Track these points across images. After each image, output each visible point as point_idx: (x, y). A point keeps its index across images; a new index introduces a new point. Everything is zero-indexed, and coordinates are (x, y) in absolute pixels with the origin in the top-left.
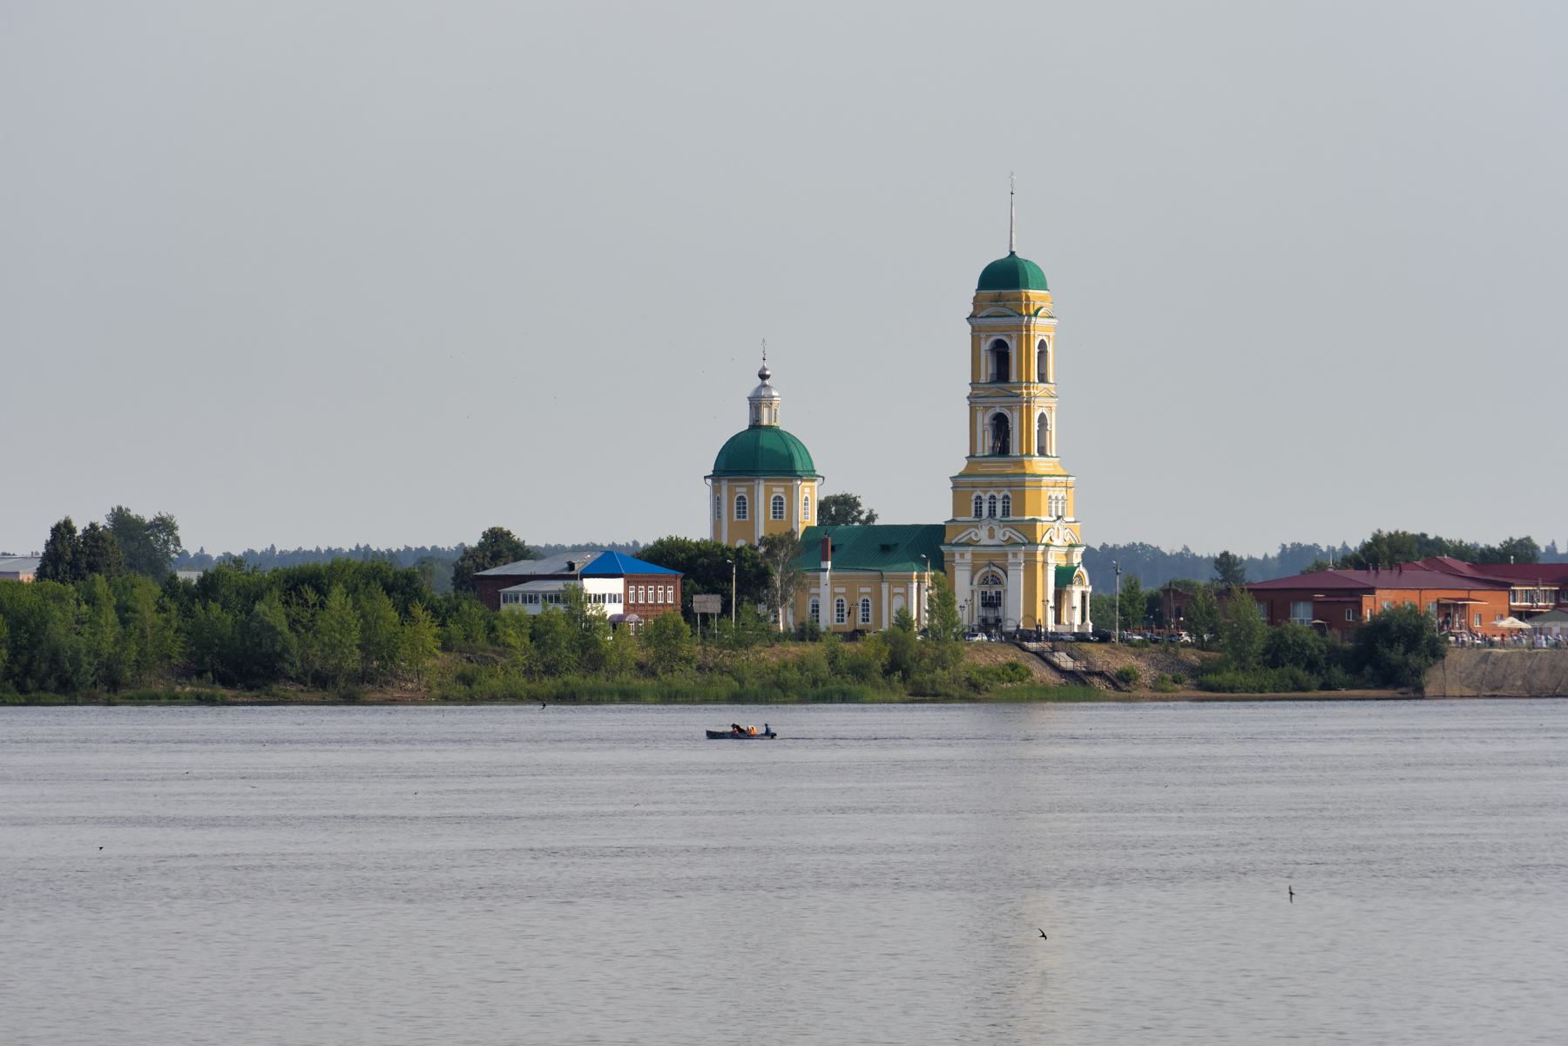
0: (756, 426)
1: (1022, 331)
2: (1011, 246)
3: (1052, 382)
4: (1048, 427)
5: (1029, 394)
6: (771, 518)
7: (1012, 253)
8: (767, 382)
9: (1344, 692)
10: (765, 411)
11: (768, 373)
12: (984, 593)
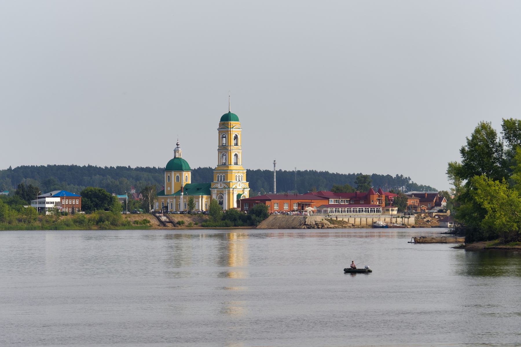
0: (175, 158)
1: (228, 132)
2: (229, 110)
3: (239, 145)
4: (238, 157)
5: (230, 149)
6: (176, 181)
7: (230, 112)
8: (178, 146)
9: (240, 227)
10: (177, 154)
11: (179, 144)
12: (219, 201)
